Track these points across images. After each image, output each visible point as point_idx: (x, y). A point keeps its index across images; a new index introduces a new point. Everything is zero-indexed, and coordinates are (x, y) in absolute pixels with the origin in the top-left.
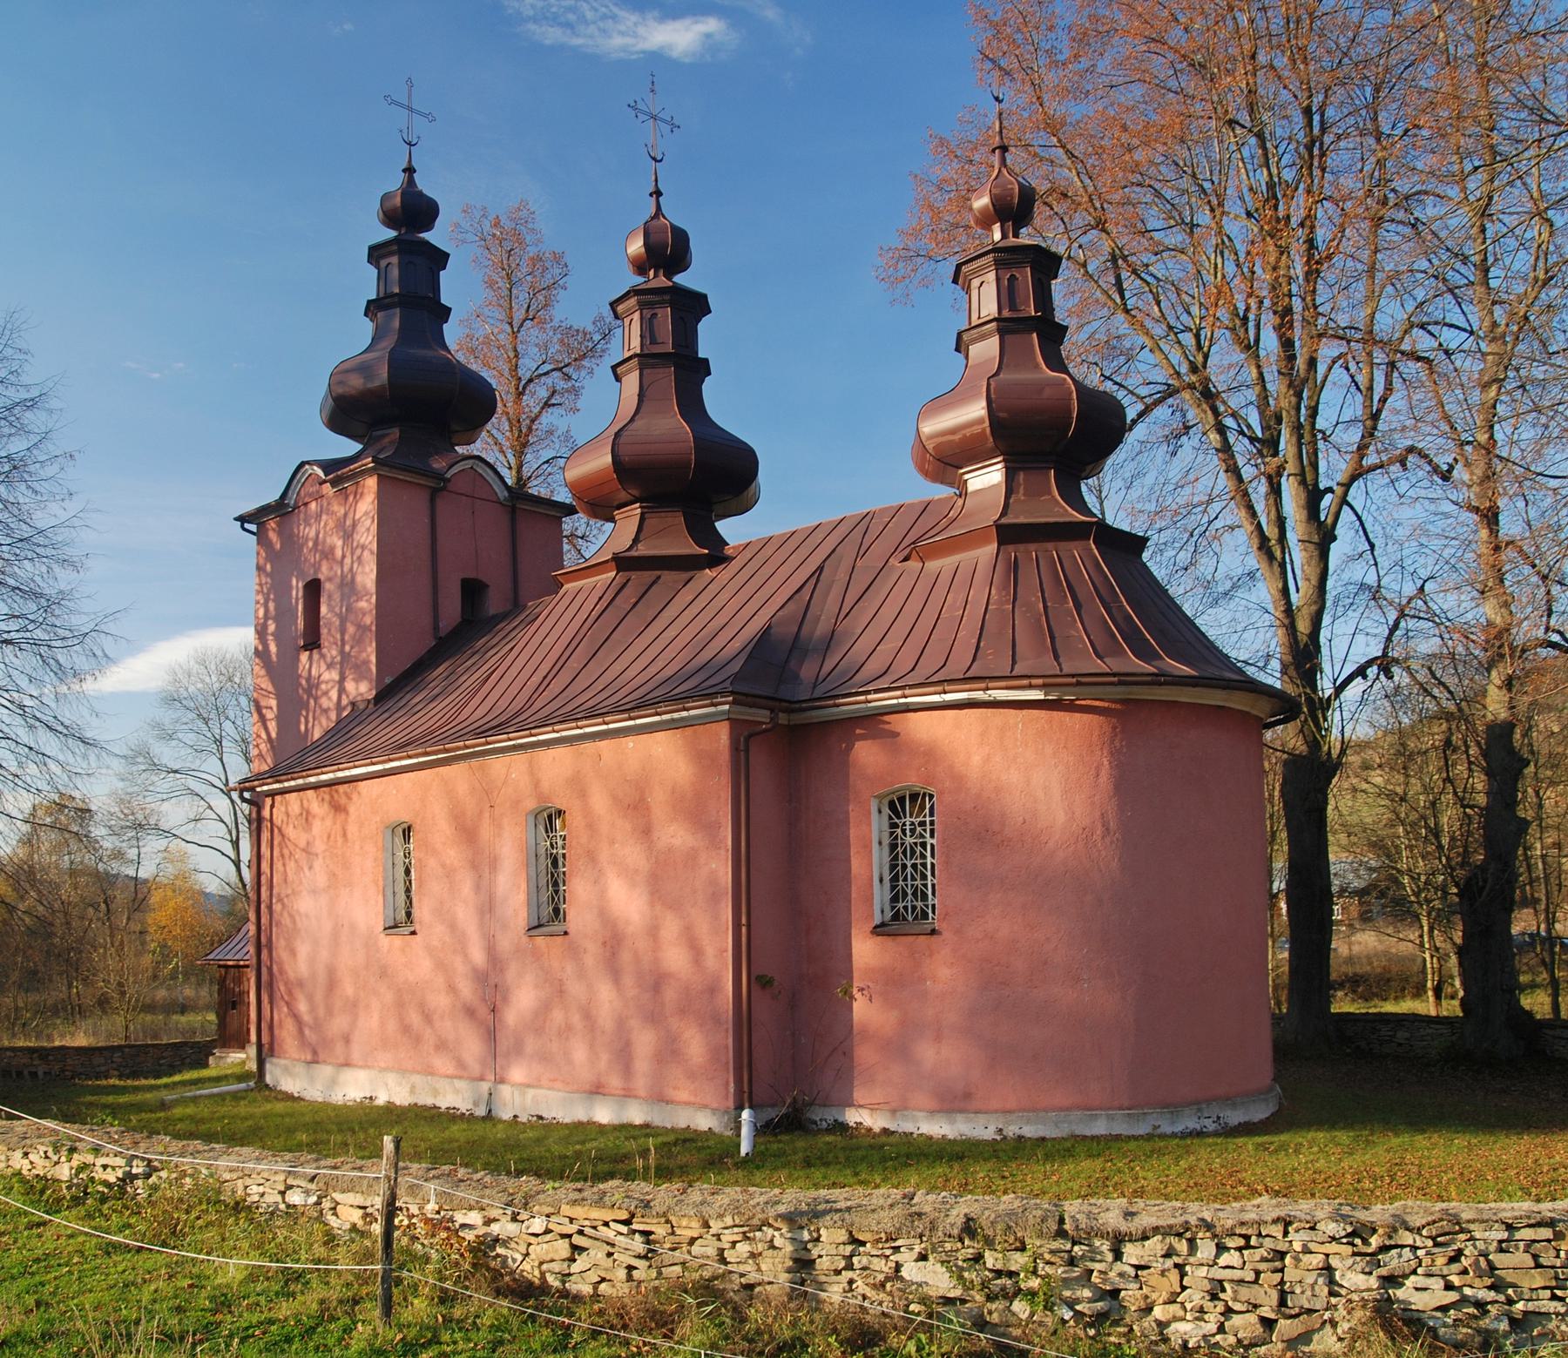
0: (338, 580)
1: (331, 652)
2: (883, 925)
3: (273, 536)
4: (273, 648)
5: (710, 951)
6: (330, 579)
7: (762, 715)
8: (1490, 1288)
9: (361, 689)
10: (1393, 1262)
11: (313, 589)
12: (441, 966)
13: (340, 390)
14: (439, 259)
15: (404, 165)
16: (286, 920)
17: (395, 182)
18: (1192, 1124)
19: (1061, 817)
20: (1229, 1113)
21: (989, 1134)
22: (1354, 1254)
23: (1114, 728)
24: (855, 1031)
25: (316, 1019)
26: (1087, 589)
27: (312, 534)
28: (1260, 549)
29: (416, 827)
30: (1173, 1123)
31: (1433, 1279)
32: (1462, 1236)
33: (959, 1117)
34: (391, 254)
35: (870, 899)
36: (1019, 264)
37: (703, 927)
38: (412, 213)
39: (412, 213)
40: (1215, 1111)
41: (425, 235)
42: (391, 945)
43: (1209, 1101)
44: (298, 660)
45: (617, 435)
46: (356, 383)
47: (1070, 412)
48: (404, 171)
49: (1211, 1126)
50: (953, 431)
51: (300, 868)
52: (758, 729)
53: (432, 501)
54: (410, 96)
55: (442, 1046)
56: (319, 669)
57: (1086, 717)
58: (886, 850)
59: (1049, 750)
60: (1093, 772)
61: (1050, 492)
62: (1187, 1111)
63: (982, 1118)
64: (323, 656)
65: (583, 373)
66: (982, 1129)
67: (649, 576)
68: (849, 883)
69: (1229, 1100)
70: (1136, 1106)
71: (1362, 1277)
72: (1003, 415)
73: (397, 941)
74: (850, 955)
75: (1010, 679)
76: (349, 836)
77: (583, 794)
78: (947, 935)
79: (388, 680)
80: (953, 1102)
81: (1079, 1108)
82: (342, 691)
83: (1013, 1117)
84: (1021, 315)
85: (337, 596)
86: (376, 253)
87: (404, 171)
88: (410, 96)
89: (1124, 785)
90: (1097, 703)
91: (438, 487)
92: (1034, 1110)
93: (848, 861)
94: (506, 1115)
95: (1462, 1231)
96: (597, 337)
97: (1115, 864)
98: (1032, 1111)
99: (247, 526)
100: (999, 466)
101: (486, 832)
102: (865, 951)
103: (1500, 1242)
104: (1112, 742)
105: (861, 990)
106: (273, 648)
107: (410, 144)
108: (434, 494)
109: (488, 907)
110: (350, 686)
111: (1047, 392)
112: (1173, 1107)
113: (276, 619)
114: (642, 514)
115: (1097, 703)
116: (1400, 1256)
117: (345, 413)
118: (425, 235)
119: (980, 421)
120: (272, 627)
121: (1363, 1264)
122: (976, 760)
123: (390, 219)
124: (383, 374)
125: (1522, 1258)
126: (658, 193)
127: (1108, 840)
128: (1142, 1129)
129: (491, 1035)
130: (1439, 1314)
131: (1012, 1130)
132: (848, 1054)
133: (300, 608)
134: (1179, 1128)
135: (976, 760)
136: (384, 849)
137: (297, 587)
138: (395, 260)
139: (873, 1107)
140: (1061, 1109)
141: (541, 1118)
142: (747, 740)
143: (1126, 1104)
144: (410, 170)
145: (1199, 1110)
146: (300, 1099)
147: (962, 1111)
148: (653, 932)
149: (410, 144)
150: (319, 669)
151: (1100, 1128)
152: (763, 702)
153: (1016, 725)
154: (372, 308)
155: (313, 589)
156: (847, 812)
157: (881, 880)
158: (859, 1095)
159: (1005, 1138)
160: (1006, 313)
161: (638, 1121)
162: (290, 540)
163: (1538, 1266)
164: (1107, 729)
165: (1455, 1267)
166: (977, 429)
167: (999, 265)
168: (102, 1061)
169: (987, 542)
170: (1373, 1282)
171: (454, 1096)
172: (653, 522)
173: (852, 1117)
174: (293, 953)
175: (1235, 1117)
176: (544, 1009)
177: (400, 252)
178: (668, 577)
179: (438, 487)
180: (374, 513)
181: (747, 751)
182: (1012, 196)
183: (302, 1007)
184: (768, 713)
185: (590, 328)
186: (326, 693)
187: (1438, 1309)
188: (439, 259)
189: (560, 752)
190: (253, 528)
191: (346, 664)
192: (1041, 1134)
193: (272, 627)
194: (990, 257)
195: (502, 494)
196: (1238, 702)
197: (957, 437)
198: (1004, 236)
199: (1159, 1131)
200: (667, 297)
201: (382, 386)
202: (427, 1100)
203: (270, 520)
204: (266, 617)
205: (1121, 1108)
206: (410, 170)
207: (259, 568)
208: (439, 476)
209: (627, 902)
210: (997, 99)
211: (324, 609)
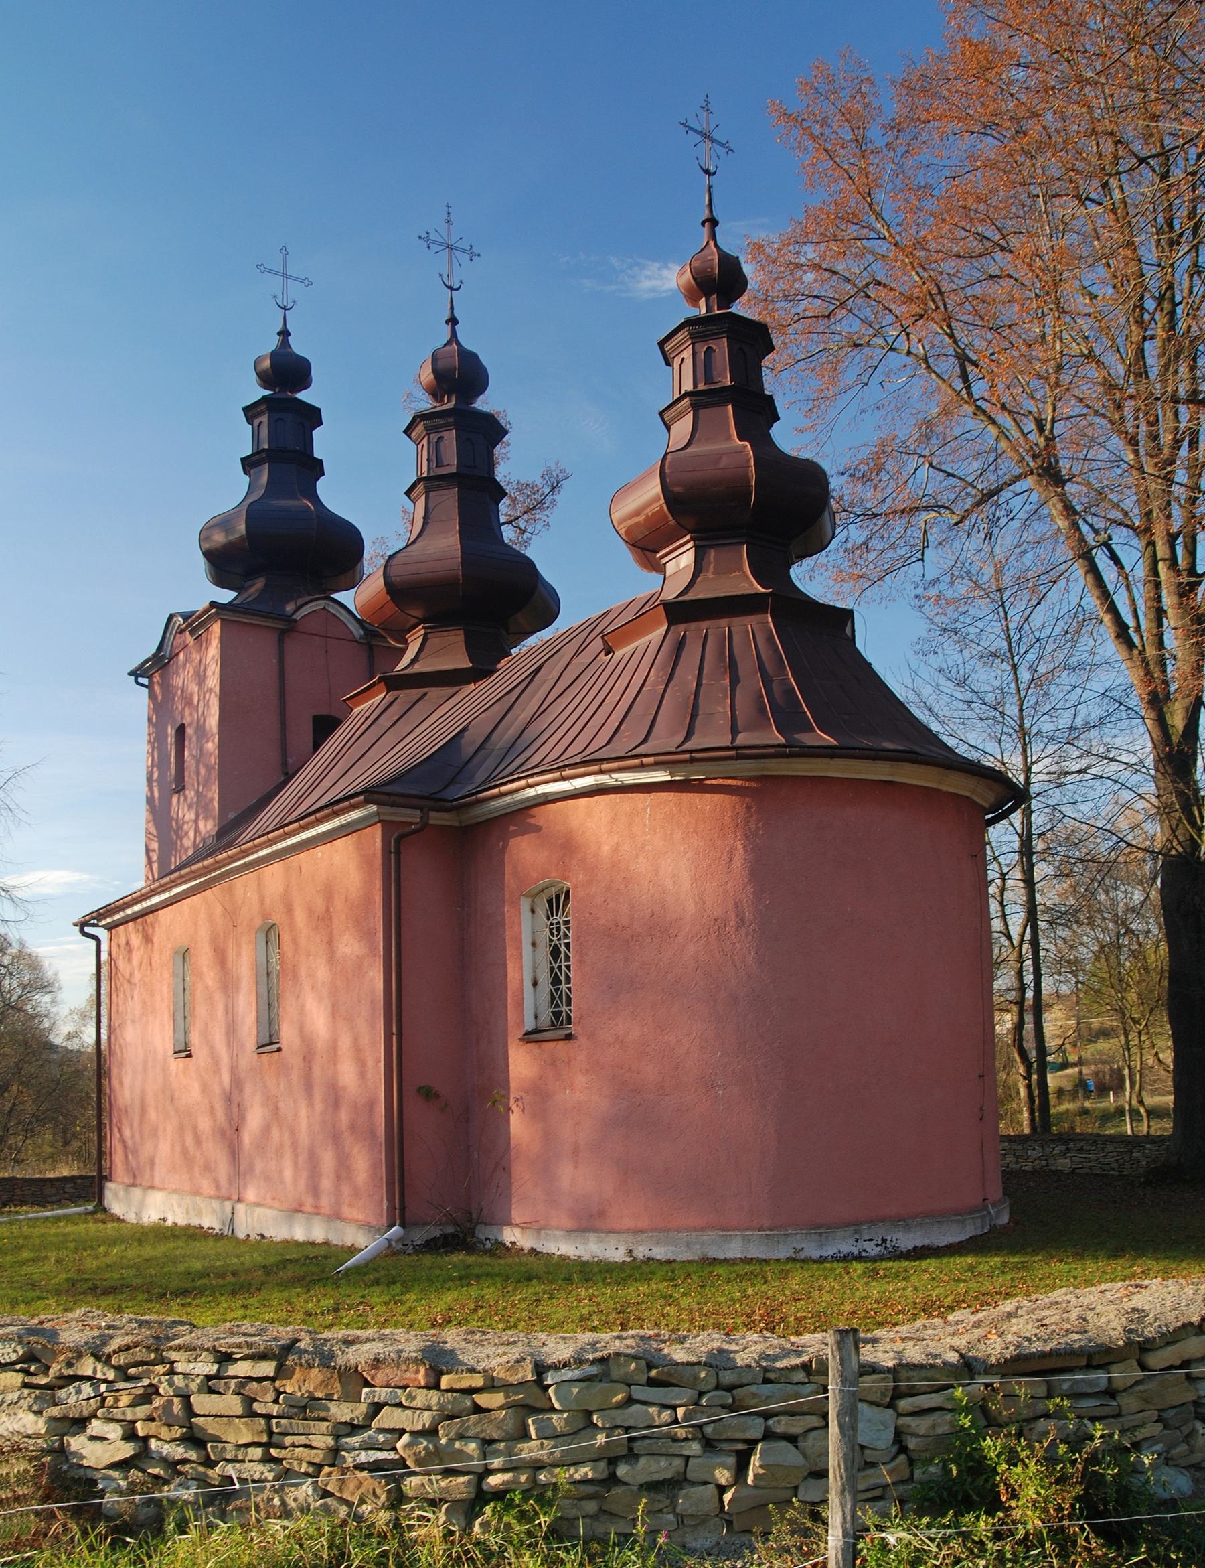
0: (195, 725)
1: (190, 794)
2: (536, 1031)
3: (157, 688)
4: (156, 794)
5: (370, 1063)
6: (190, 725)
7: (413, 816)
8: (182, 1440)
9: (208, 827)
10: (75, 1399)
11: (181, 731)
12: (205, 1089)
13: (206, 546)
14: (313, 416)
15: (279, 328)
16: (118, 1050)
17: (273, 343)
18: (847, 1247)
19: (691, 907)
20: (900, 1235)
21: (618, 1255)
22: (26, 1385)
23: (749, 808)
24: (512, 1142)
25: (134, 1143)
26: (747, 667)
27: (180, 684)
28: (1118, 637)
29: (192, 951)
30: (821, 1246)
31: (112, 1426)
32: (160, 1369)
33: (592, 1237)
34: (261, 413)
35: (520, 1004)
36: (715, 335)
37: (365, 1040)
38: (286, 373)
39: (286, 373)
40: (879, 1232)
41: (302, 396)
42: (176, 1065)
43: (872, 1222)
44: (170, 802)
45: (391, 557)
46: (219, 538)
47: (749, 481)
48: (279, 334)
49: (872, 1249)
50: (637, 513)
51: (126, 999)
52: (406, 830)
53: (281, 641)
54: (284, 265)
55: (207, 1168)
56: (183, 810)
57: (717, 798)
58: (544, 952)
59: (678, 836)
60: (725, 857)
61: (741, 569)
62: (840, 1233)
63: (613, 1240)
64: (186, 798)
65: (539, 526)
66: (614, 1251)
67: (415, 693)
68: (506, 988)
69: (903, 1221)
70: (776, 1229)
71: (32, 1416)
72: (677, 489)
73: (181, 1063)
74: (507, 1066)
75: (633, 759)
76: (154, 964)
77: (289, 910)
78: (582, 1040)
79: (231, 816)
80: (588, 1221)
81: (713, 1228)
82: (197, 830)
83: (643, 1237)
84: (719, 386)
85: (194, 739)
86: (250, 412)
87: (279, 334)
88: (284, 265)
89: (762, 870)
90: (729, 782)
91: (288, 628)
92: (667, 1230)
93: (505, 965)
94: (241, 1235)
95: (162, 1361)
96: (547, 490)
97: (751, 958)
98: (663, 1231)
99: (140, 680)
100: (690, 544)
101: (231, 954)
102: (521, 1064)
103: (208, 1378)
104: (747, 823)
105: (517, 1100)
106: (156, 794)
107: (285, 309)
108: (283, 634)
109: (231, 1030)
110: (201, 824)
111: (724, 462)
112: (821, 1229)
113: (159, 769)
114: (425, 635)
115: (729, 782)
116: (79, 1391)
117: (223, 563)
118: (302, 396)
119: (656, 499)
120: (156, 775)
121: (30, 1400)
122: (606, 849)
123: (265, 379)
124: (242, 528)
125: (232, 1403)
126: (453, 321)
127: (743, 931)
128: (784, 1252)
129: (234, 1152)
130: (115, 1474)
131: (641, 1252)
132: (507, 1170)
133: (173, 754)
134: (829, 1251)
135: (606, 849)
136: (174, 974)
137: (171, 731)
138: (264, 419)
139: (523, 1227)
140: (695, 1229)
141: (263, 1236)
142: (398, 841)
143: (767, 1223)
144: (284, 333)
145: (856, 1232)
146: (123, 1221)
147: (595, 1230)
148: (333, 1047)
149: (285, 309)
150: (183, 810)
151: (735, 1249)
152: (415, 802)
153: (645, 809)
154: (248, 464)
155: (181, 731)
156: (503, 914)
157: (535, 984)
158: (517, 1215)
159: (635, 1259)
160: (701, 387)
161: (320, 1240)
162: (166, 686)
163: (251, 1414)
164: (741, 809)
165: (142, 1411)
166: (655, 507)
167: (695, 338)
168: (54, 1191)
169: (658, 624)
170: (40, 1425)
171: (208, 1221)
172: (435, 641)
173: (510, 1236)
174: (121, 1083)
175: (907, 1240)
176: (266, 1130)
177: (271, 410)
178: (435, 693)
179: (288, 628)
180: (218, 657)
181: (398, 853)
182: (712, 268)
183: (127, 1133)
184: (418, 812)
185: (539, 482)
186: (187, 833)
187: (115, 1466)
188: (313, 416)
189: (276, 868)
190: (145, 681)
191: (201, 807)
192: (671, 1256)
193: (156, 775)
194: (684, 333)
195: (357, 632)
196: (955, 784)
197: (641, 519)
198: (709, 309)
199: (802, 1255)
200: (451, 420)
201: (241, 538)
202: (195, 1222)
203: (155, 669)
204: (152, 766)
205: (760, 1229)
206: (284, 333)
207: (150, 720)
208: (288, 619)
209: (319, 1020)
210: (707, 172)
211: (186, 753)
